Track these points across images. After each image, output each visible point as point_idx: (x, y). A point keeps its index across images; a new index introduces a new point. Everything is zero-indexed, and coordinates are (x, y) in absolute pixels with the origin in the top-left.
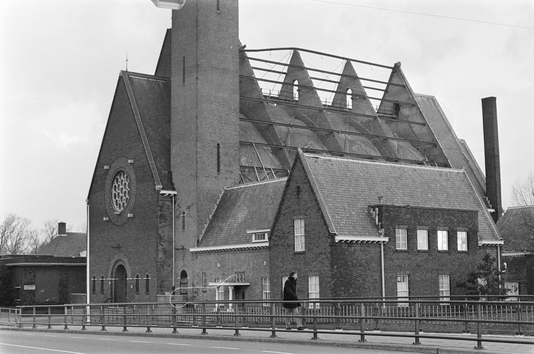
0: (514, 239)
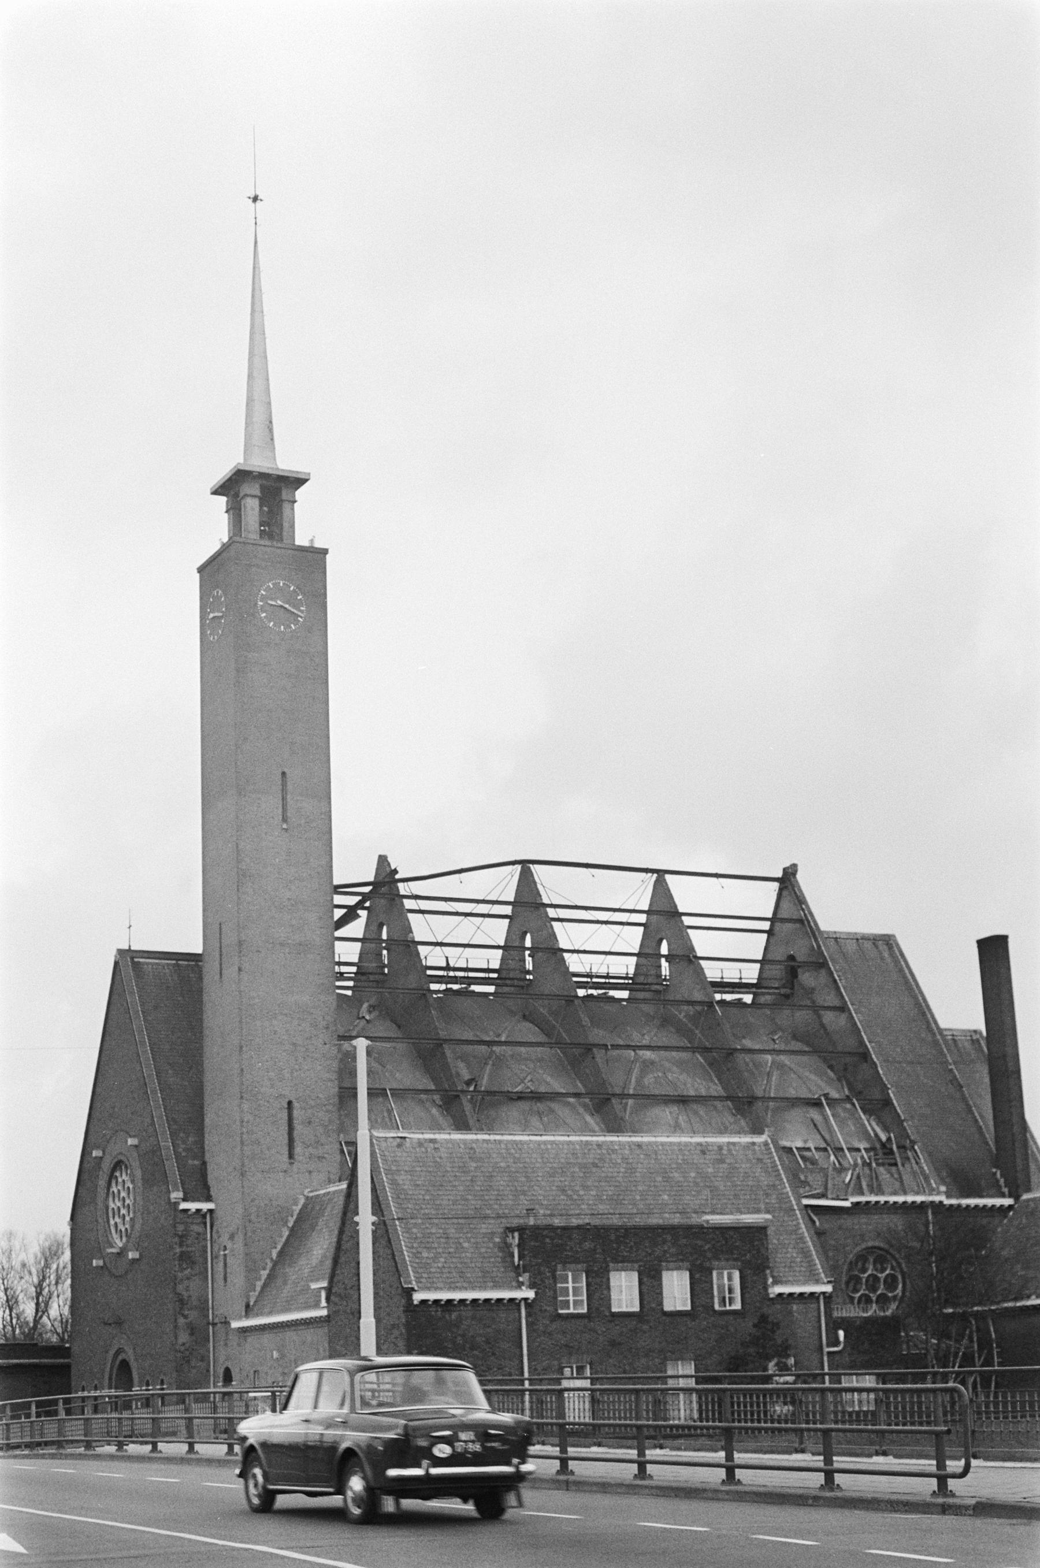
0: (1023, 1269)
